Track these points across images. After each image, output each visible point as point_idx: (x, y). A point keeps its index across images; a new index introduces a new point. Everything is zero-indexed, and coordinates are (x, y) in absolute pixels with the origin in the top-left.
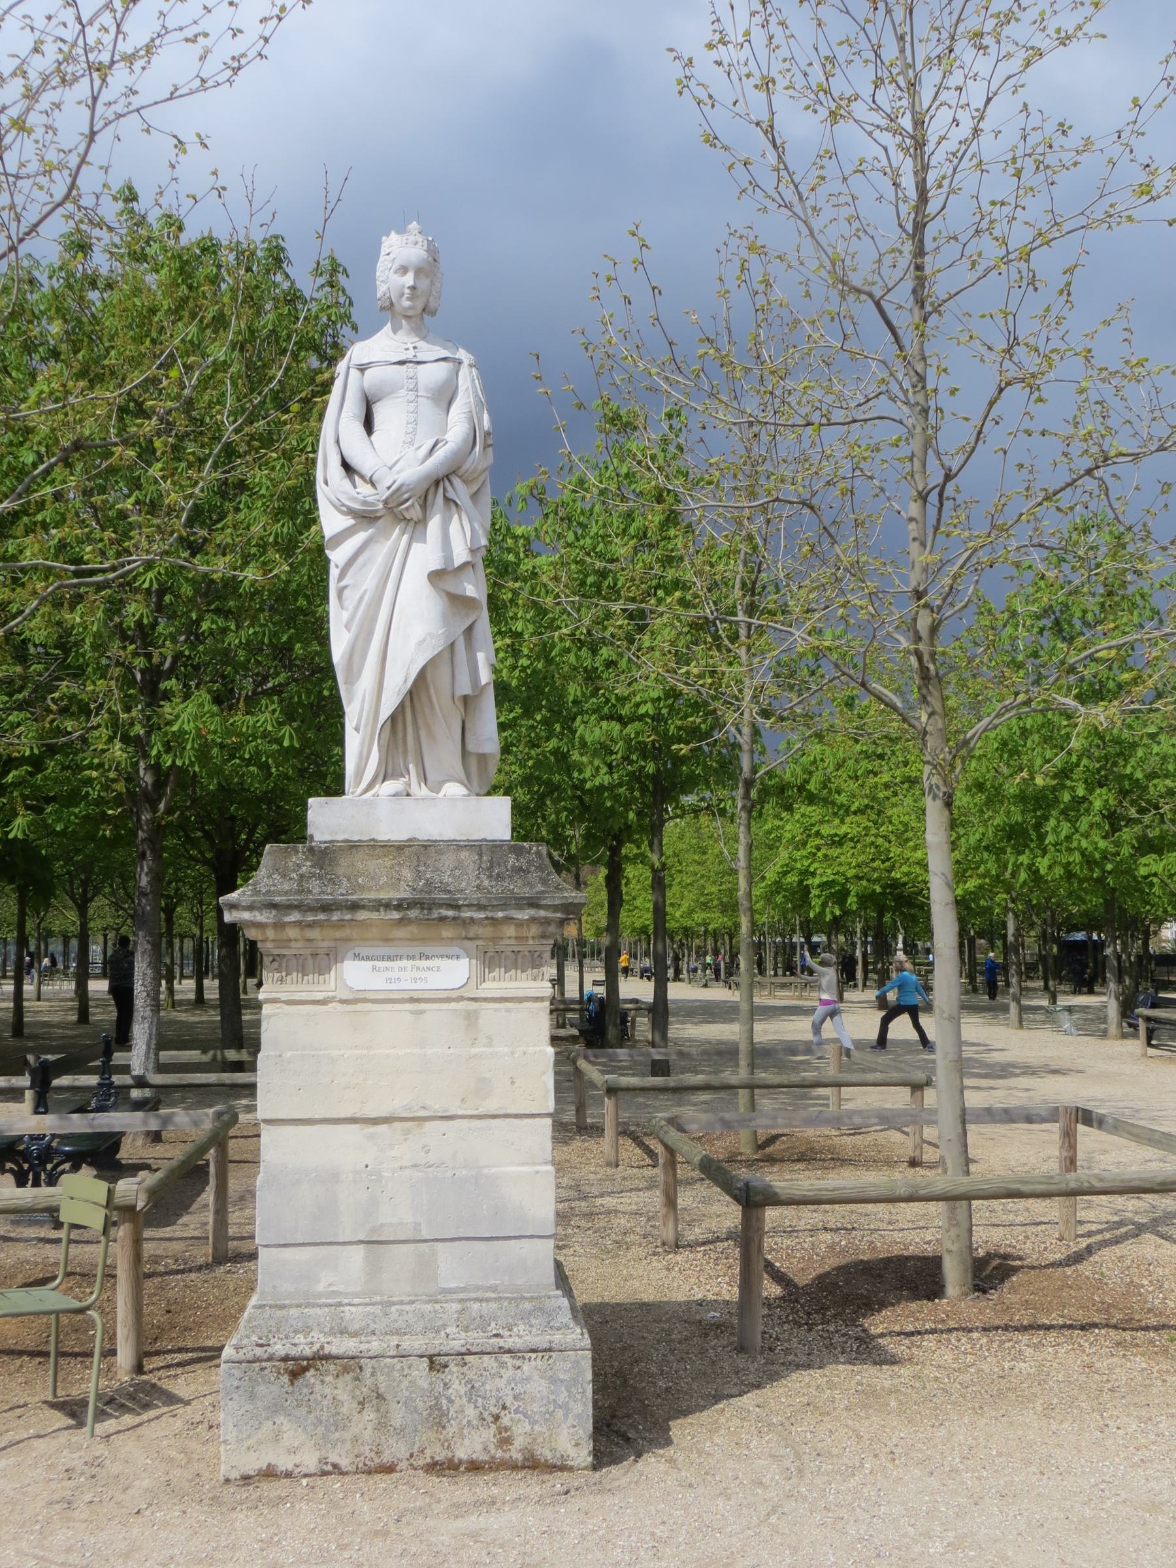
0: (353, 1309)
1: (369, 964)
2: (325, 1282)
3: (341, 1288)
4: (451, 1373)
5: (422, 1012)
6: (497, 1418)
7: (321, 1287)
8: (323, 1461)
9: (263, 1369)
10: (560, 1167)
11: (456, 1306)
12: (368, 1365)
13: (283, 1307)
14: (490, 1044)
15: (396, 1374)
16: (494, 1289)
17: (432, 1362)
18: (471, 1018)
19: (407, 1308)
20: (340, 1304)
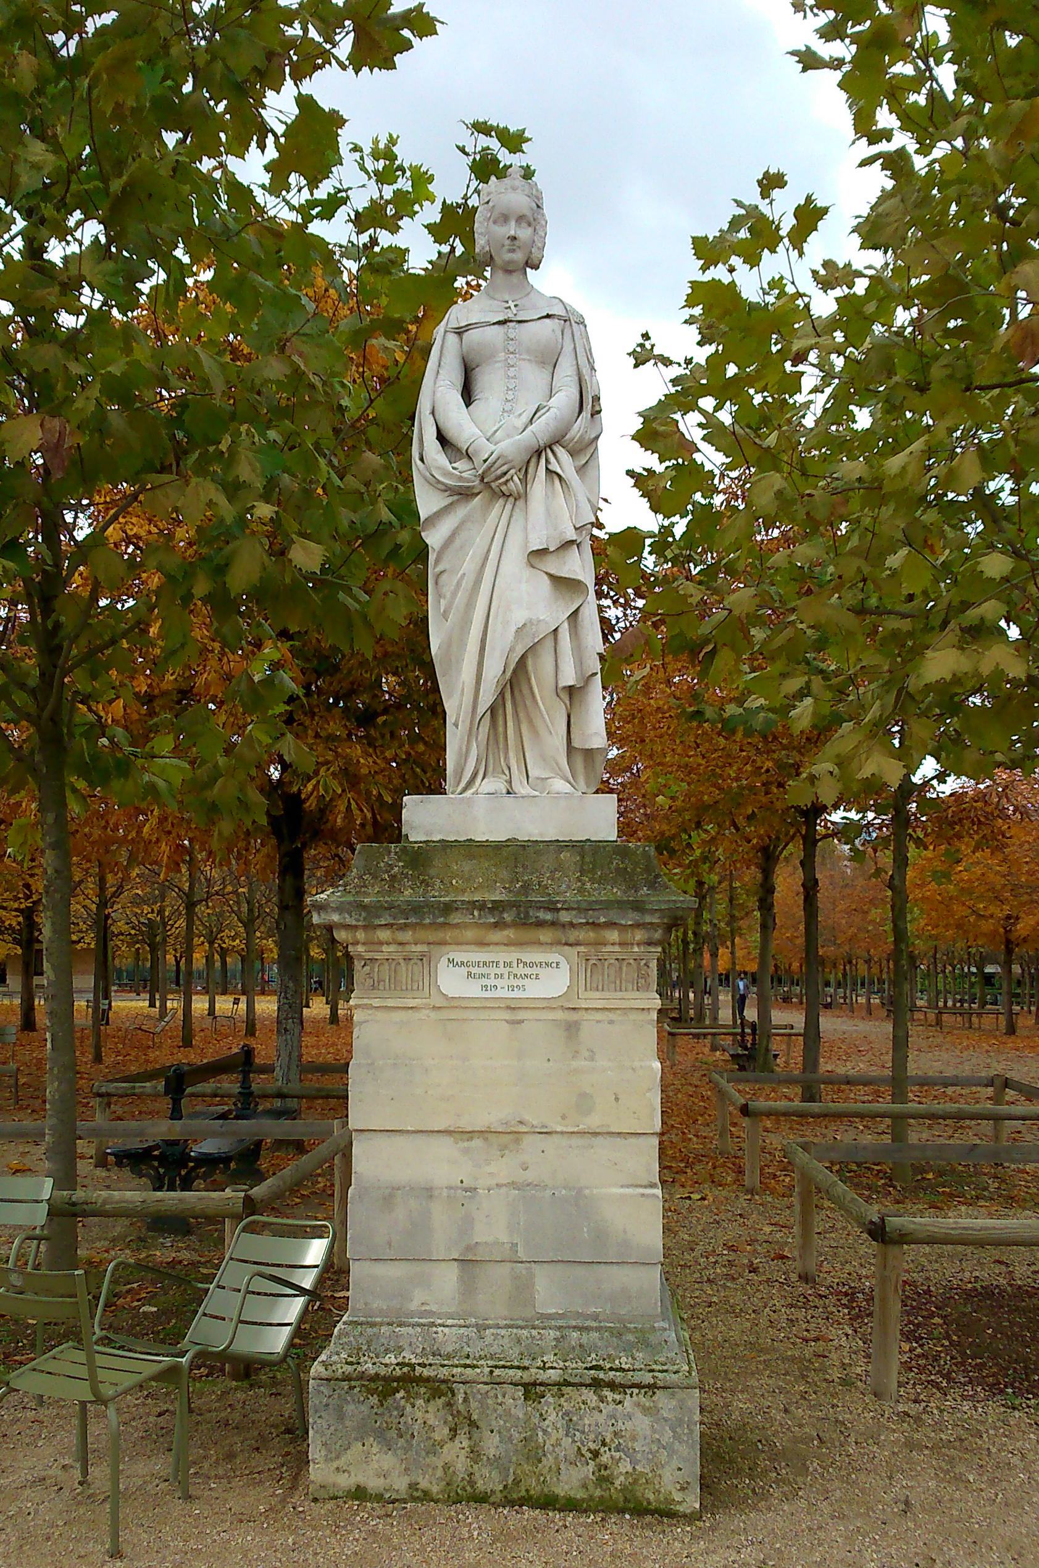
0: (446, 1330)
1: (464, 971)
2: (418, 1299)
5: (521, 1022)
7: (414, 1306)
8: (413, 1486)
9: (352, 1388)
12: (460, 1389)
13: (373, 1325)
14: (592, 1059)
16: (595, 1317)
18: (572, 1029)
19: (503, 1332)
20: (433, 1324)
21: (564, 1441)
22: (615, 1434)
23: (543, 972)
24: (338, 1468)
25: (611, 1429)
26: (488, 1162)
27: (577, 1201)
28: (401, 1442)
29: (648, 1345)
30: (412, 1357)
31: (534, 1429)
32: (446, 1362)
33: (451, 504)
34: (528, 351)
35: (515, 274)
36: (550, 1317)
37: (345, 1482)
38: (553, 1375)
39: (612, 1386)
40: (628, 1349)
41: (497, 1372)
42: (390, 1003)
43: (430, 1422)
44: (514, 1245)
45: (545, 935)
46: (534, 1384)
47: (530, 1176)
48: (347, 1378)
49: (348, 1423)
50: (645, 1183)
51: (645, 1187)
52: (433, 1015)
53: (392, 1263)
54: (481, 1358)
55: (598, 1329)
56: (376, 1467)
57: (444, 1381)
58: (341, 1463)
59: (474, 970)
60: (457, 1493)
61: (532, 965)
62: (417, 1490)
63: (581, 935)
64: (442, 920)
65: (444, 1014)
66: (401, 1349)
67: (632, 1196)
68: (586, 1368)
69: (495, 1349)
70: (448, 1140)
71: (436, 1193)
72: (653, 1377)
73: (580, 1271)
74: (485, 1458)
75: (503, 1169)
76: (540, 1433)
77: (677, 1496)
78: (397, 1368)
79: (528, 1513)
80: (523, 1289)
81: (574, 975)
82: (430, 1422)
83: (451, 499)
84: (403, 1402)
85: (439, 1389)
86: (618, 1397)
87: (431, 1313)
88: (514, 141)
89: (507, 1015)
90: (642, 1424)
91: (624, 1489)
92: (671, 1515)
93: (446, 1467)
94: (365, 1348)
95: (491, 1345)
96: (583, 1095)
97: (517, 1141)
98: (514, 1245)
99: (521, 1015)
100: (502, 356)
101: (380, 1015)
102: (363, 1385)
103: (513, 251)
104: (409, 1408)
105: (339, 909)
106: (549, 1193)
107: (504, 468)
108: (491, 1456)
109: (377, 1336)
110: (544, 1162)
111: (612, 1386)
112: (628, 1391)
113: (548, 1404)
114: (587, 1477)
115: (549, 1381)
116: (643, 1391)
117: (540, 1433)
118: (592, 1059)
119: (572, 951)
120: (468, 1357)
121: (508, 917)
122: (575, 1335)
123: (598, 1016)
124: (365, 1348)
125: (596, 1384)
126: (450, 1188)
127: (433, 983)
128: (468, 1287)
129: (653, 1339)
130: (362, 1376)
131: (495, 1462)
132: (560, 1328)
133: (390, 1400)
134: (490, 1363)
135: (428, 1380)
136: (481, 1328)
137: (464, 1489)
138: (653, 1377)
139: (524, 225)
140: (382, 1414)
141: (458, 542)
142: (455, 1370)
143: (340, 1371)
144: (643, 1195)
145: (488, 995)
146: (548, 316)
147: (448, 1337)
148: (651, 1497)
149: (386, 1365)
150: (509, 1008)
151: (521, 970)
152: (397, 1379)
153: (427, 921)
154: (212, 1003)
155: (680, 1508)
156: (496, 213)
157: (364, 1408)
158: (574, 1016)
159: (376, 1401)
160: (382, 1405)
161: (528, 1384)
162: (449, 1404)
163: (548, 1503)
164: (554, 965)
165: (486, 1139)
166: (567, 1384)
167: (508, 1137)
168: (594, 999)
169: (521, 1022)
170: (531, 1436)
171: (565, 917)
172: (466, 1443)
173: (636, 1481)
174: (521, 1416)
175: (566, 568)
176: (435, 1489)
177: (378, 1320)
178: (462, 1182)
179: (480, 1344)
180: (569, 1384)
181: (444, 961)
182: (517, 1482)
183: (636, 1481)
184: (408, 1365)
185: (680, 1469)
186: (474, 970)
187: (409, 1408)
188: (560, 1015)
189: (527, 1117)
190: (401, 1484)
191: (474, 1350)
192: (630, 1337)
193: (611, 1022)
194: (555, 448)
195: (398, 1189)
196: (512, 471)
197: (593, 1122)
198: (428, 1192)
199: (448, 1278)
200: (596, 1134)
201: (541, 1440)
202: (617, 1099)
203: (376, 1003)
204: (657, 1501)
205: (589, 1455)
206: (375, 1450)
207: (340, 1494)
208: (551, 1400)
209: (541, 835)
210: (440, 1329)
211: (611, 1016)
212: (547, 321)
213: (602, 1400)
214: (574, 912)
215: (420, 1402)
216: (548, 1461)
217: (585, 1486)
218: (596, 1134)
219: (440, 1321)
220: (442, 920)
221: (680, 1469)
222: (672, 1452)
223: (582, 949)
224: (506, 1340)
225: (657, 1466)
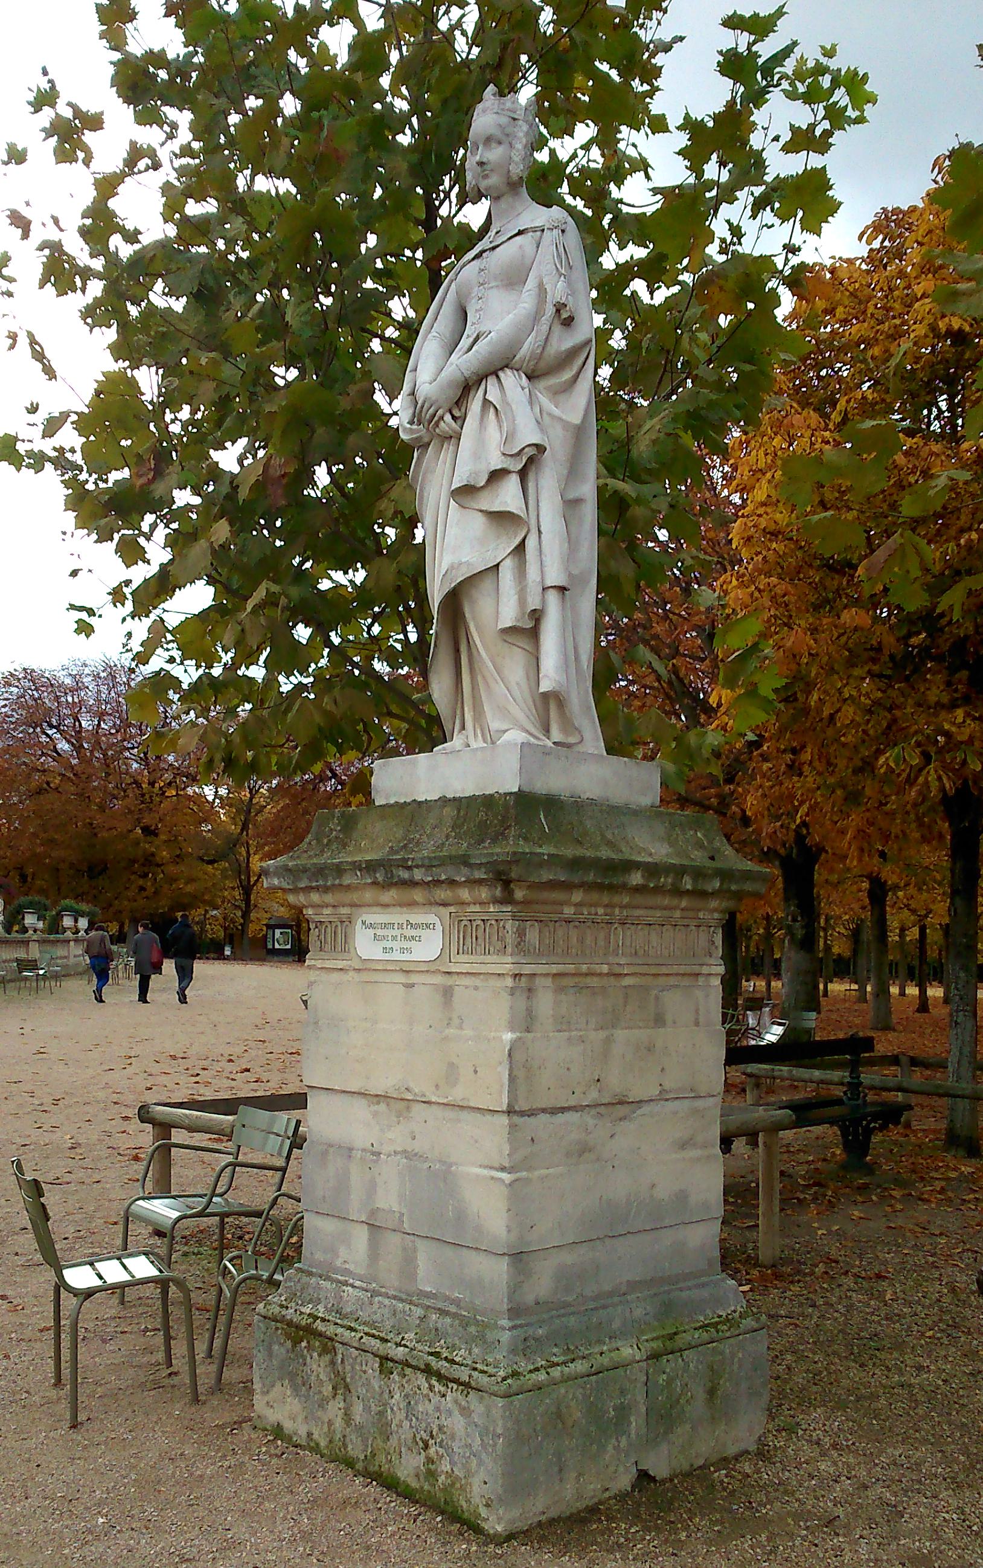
1: (371, 932)
3: (350, 1267)
5: (413, 985)
9: (277, 1329)
13: (310, 1274)
14: (461, 1028)
16: (457, 1302)
18: (447, 993)
19: (387, 1302)
20: (346, 1283)
25: (437, 1422)
26: (389, 1127)
27: (443, 1176)
29: (485, 1342)
32: (339, 1321)
34: (495, 279)
35: (503, 199)
39: (440, 1377)
40: (469, 1341)
45: (418, 895)
47: (416, 1146)
50: (497, 1165)
51: (497, 1169)
55: (455, 1316)
56: (279, 1406)
59: (379, 932)
63: (442, 894)
64: (337, 882)
65: (365, 976)
67: (484, 1177)
70: (363, 1102)
73: (449, 1252)
75: (396, 1137)
77: (483, 1512)
79: (374, 1489)
80: (409, 1260)
81: (447, 935)
85: (328, 1346)
88: (760, 26)
89: (401, 978)
90: (457, 1423)
92: (478, 1530)
96: (452, 1066)
99: (414, 979)
103: (486, 177)
106: (426, 1165)
107: (431, 411)
110: (430, 1132)
111: (440, 1377)
112: (450, 1385)
114: (419, 1467)
116: (461, 1388)
118: (461, 1028)
119: (445, 911)
121: (380, 877)
125: (428, 1371)
126: (364, 1150)
129: (490, 1336)
134: (366, 1329)
135: (320, 1335)
136: (375, 1293)
139: (494, 145)
142: (340, 1330)
144: (492, 1178)
145: (387, 957)
146: (520, 233)
154: (769, 985)
155: (485, 1526)
158: (449, 981)
164: (396, 926)
168: (462, 963)
169: (413, 985)
171: (418, 875)
172: (342, 1405)
173: (453, 1484)
175: (497, 502)
176: (323, 1444)
180: (409, 1366)
181: (359, 922)
183: (453, 1484)
185: (485, 1483)
186: (379, 932)
188: (438, 979)
189: (412, 1085)
193: (476, 988)
194: (501, 374)
196: (440, 412)
197: (457, 1094)
198: (349, 1151)
202: (476, 1072)
205: (421, 1444)
208: (397, 1378)
209: (463, 790)
212: (518, 238)
213: (431, 1388)
216: (393, 1441)
219: (351, 1281)
221: (485, 1483)
222: (481, 1463)
223: (452, 909)
224: (387, 1310)
225: (469, 1474)
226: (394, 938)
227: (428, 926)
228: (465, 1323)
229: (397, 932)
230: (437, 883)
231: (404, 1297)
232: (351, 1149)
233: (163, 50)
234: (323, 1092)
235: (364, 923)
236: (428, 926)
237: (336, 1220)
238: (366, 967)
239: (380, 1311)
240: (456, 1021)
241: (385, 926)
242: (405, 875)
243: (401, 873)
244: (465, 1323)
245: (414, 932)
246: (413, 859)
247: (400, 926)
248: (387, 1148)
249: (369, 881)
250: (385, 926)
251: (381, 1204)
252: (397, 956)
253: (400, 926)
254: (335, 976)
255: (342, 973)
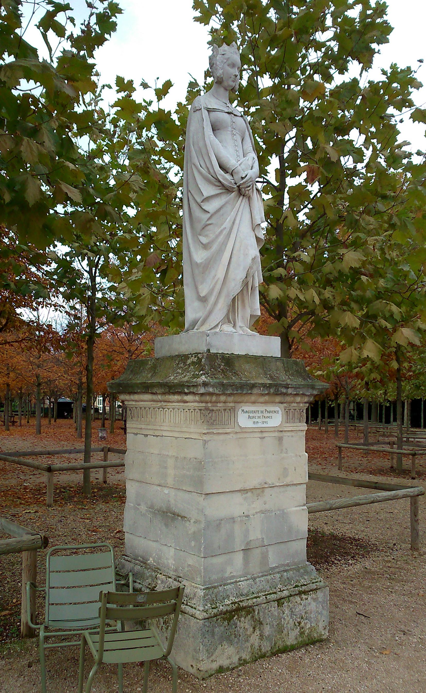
0: (243, 583)
1: (247, 415)
2: (229, 571)
3: (235, 574)
4: (285, 606)
5: (264, 438)
6: (299, 623)
7: (227, 575)
8: (240, 659)
9: (217, 620)
10: (126, 447)
11: (278, 576)
12: (256, 608)
13: (215, 587)
14: (287, 453)
15: (266, 611)
16: (288, 565)
17: (278, 603)
18: (280, 439)
19: (262, 579)
20: (236, 582)
21: (288, 622)
22: (306, 613)
23: (273, 415)
24: (212, 661)
26: (253, 502)
27: (283, 515)
28: (236, 640)
30: (234, 598)
31: (280, 619)
33: (221, 193)
36: (274, 568)
37: (215, 666)
38: (286, 593)
39: (305, 592)
41: (268, 597)
42: (221, 431)
43: (246, 627)
44: (263, 538)
45: (278, 399)
46: (281, 599)
47: (267, 507)
48: (215, 616)
49: (216, 637)
50: (302, 504)
52: (235, 436)
53: (220, 556)
54: (258, 593)
55: (291, 570)
57: (250, 607)
58: (213, 657)
59: (251, 415)
60: (255, 656)
61: (269, 412)
62: (241, 660)
65: (239, 436)
66: (228, 596)
68: (294, 587)
69: (261, 587)
70: (239, 494)
71: (236, 519)
72: (316, 585)
73: (283, 546)
74: (265, 637)
75: (258, 505)
76: (283, 620)
78: (233, 605)
80: (265, 557)
82: (246, 627)
83: (221, 191)
84: (236, 621)
85: (249, 610)
86: (306, 597)
87: (233, 577)
89: (259, 435)
91: (309, 635)
93: (252, 646)
94: (215, 599)
95: (259, 586)
96: (285, 469)
97: (263, 492)
98: (263, 538)
99: (265, 435)
100: (230, 129)
101: (216, 437)
102: (221, 617)
104: (238, 623)
105: (213, 386)
108: (267, 636)
109: (218, 592)
110: (272, 500)
113: (285, 606)
115: (285, 596)
117: (283, 620)
118: (287, 453)
120: (253, 593)
121: (272, 391)
122: (285, 574)
123: (289, 434)
124: (215, 599)
125: (300, 593)
127: (236, 421)
128: (246, 561)
130: (222, 613)
131: (269, 638)
132: (278, 572)
133: (232, 621)
134: (263, 594)
137: (258, 654)
138: (316, 585)
140: (229, 629)
141: (221, 212)
143: (213, 613)
144: (303, 509)
147: (244, 585)
148: (315, 635)
149: (228, 605)
150: (262, 432)
151: (267, 415)
152: (234, 611)
153: (245, 392)
156: (229, 62)
157: (222, 628)
159: (227, 623)
160: (229, 624)
161: (278, 600)
162: (253, 617)
163: (286, 650)
164: (260, 412)
165: (252, 492)
166: (291, 596)
167: (258, 491)
168: (289, 427)
169: (264, 438)
170: (280, 623)
171: (290, 391)
174: (276, 614)
177: (216, 584)
178: (244, 513)
179: (256, 586)
181: (240, 410)
182: (275, 644)
184: (236, 603)
186: (251, 415)
187: (238, 623)
188: (276, 434)
190: (235, 659)
191: (254, 590)
192: (302, 571)
193: (292, 436)
195: (222, 520)
197: (288, 480)
198: (232, 520)
199: (239, 558)
200: (288, 485)
201: (283, 623)
202: (295, 470)
203: (215, 431)
204: (318, 636)
206: (226, 647)
207: (213, 673)
208: (286, 604)
209: (256, 353)
210: (240, 583)
211: (293, 434)
214: (293, 389)
215: (243, 619)
217: (296, 638)
218: (288, 485)
219: (238, 580)
220: (250, 392)
223: (285, 405)
226: (259, 417)
227: (275, 412)
228: (298, 570)
229: (260, 415)
230: (297, 395)
231: (266, 574)
232: (233, 518)
233: (375, 49)
234: (215, 495)
235: (243, 411)
236: (275, 412)
237: (223, 555)
238: (244, 431)
239: (262, 583)
240: (284, 450)
241: (252, 412)
242: (284, 391)
243: (282, 390)
244: (298, 570)
245: (269, 415)
246: (291, 384)
247: (262, 412)
248: (252, 512)
249: (267, 392)
250: (252, 412)
251: (251, 538)
252: (260, 425)
253: (262, 412)
254: (222, 437)
255: (226, 435)
